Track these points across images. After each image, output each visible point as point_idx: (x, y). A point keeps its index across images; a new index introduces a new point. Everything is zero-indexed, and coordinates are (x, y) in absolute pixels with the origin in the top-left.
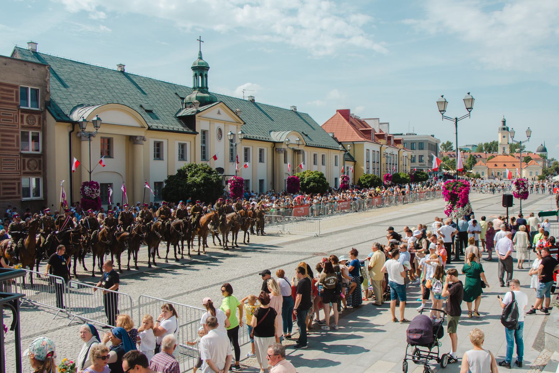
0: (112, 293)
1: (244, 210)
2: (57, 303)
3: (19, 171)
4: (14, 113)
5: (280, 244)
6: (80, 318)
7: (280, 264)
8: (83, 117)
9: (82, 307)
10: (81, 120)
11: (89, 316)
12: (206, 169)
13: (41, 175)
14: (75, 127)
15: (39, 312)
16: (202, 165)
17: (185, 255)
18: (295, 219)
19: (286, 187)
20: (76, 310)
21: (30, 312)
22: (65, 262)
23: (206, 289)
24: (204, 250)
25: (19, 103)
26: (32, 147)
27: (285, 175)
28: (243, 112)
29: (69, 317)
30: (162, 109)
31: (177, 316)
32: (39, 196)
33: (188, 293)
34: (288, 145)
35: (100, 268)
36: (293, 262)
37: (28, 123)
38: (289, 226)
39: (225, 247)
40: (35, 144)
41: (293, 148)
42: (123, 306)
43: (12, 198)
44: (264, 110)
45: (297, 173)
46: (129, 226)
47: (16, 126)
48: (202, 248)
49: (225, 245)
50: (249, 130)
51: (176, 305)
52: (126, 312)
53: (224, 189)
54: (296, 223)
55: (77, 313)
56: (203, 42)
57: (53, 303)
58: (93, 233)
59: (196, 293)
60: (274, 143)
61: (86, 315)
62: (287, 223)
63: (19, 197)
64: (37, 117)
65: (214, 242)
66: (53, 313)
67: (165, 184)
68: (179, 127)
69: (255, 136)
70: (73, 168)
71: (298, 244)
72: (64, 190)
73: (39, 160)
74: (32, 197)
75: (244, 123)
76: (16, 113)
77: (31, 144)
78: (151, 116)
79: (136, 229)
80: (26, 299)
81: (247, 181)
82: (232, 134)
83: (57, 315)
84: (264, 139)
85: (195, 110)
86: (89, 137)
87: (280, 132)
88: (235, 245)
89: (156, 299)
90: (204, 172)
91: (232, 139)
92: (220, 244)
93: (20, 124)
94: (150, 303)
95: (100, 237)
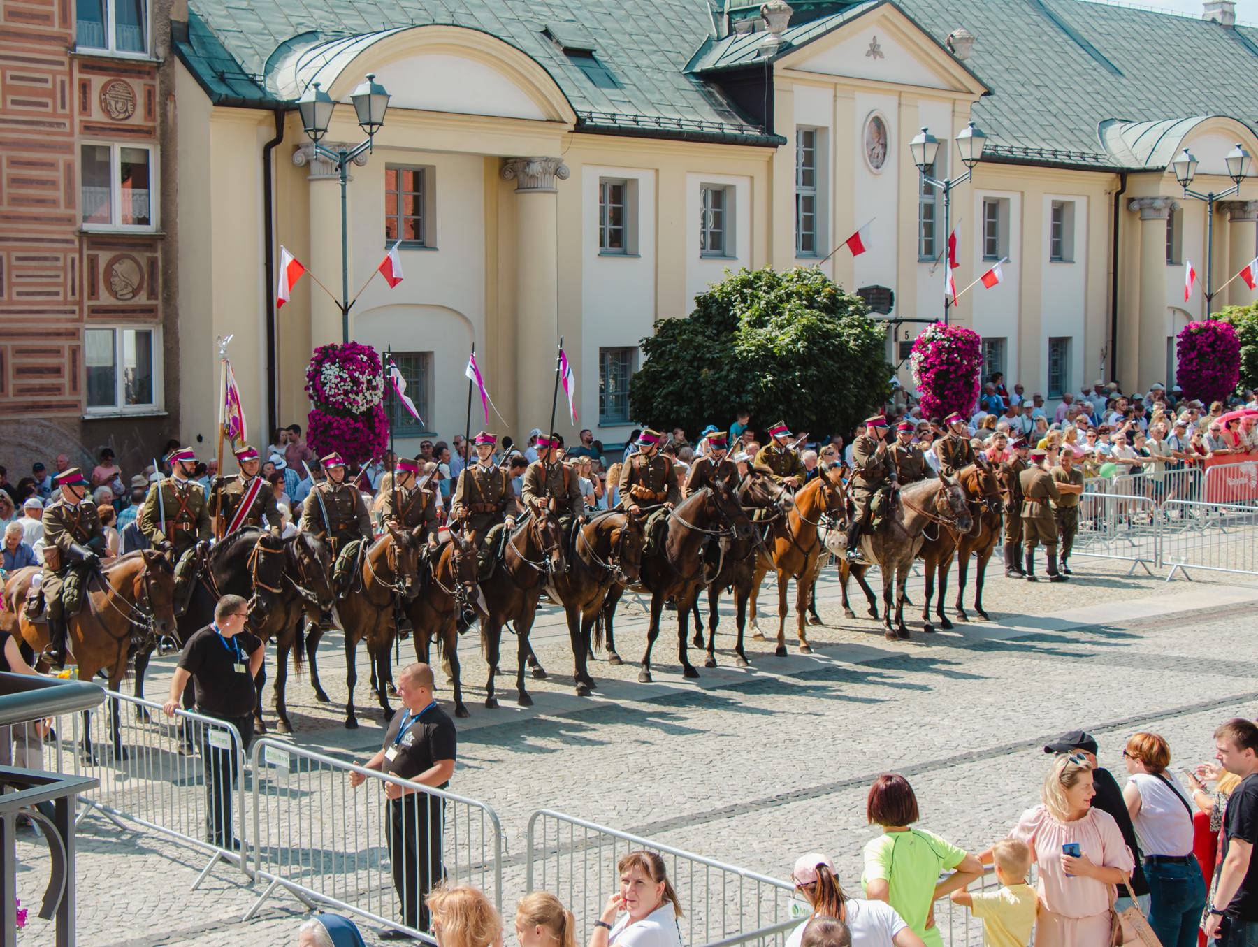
0: (422, 795)
1: (979, 465)
2: (209, 827)
3: (74, 303)
4: (54, 73)
5: (1139, 623)
6: (296, 892)
7: (1141, 710)
8: (317, 86)
9: (306, 846)
10: (309, 97)
11: (329, 883)
12: (818, 292)
13: (156, 317)
14: (286, 125)
15: (141, 858)
16: (799, 276)
17: (722, 652)
18: (1215, 515)
19: (1176, 368)
20: (281, 856)
21: (106, 856)
22: (245, 663)
23: (810, 801)
24: (802, 636)
25: (74, 32)
26: (123, 209)
27: (1168, 315)
28: (981, 39)
29: (252, 882)
30: (636, 42)
31: (677, 909)
32: (150, 401)
33: (730, 812)
34: (1185, 182)
35: (377, 693)
36: (1204, 707)
37: (107, 112)
38: (1182, 544)
39: (896, 627)
40: (133, 195)
41: (1211, 196)
42: (466, 852)
43: (48, 406)
44: (1077, 27)
45: (1228, 308)
46: (495, 528)
47: (64, 124)
48: (796, 627)
49: (892, 617)
50: (1006, 123)
51: (679, 860)
52: (476, 877)
53: (894, 379)
54: (1216, 531)
55: (285, 870)
57: (192, 827)
58: (343, 553)
59: (765, 815)
60: (1123, 174)
61: (317, 880)
62: (1174, 531)
63: (74, 406)
64: (138, 85)
65: (846, 604)
66: (194, 863)
67: (642, 358)
68: (706, 116)
69: (1035, 145)
70: (282, 290)
71: (1225, 627)
72: (230, 375)
73: (149, 258)
74: (122, 407)
75: (983, 90)
76: (61, 73)
77: (120, 197)
78: (589, 71)
79: (520, 536)
80: (93, 804)
81: (996, 344)
82: (930, 139)
83: (209, 873)
84: (1076, 160)
85: (769, 40)
86: (341, 166)
87: (1150, 124)
88: (939, 620)
89: (600, 831)
90: (807, 307)
91: (929, 161)
92: (873, 611)
93: (77, 118)
94: (574, 847)
95: (369, 568)
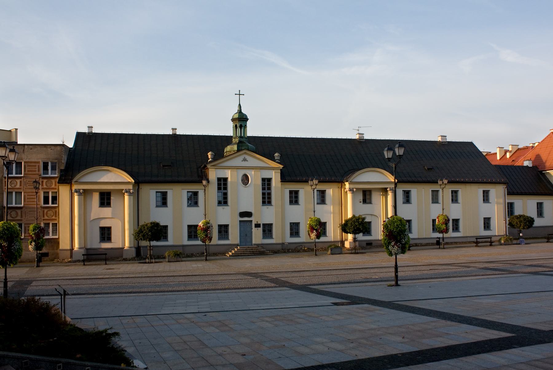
37: (47, 186)
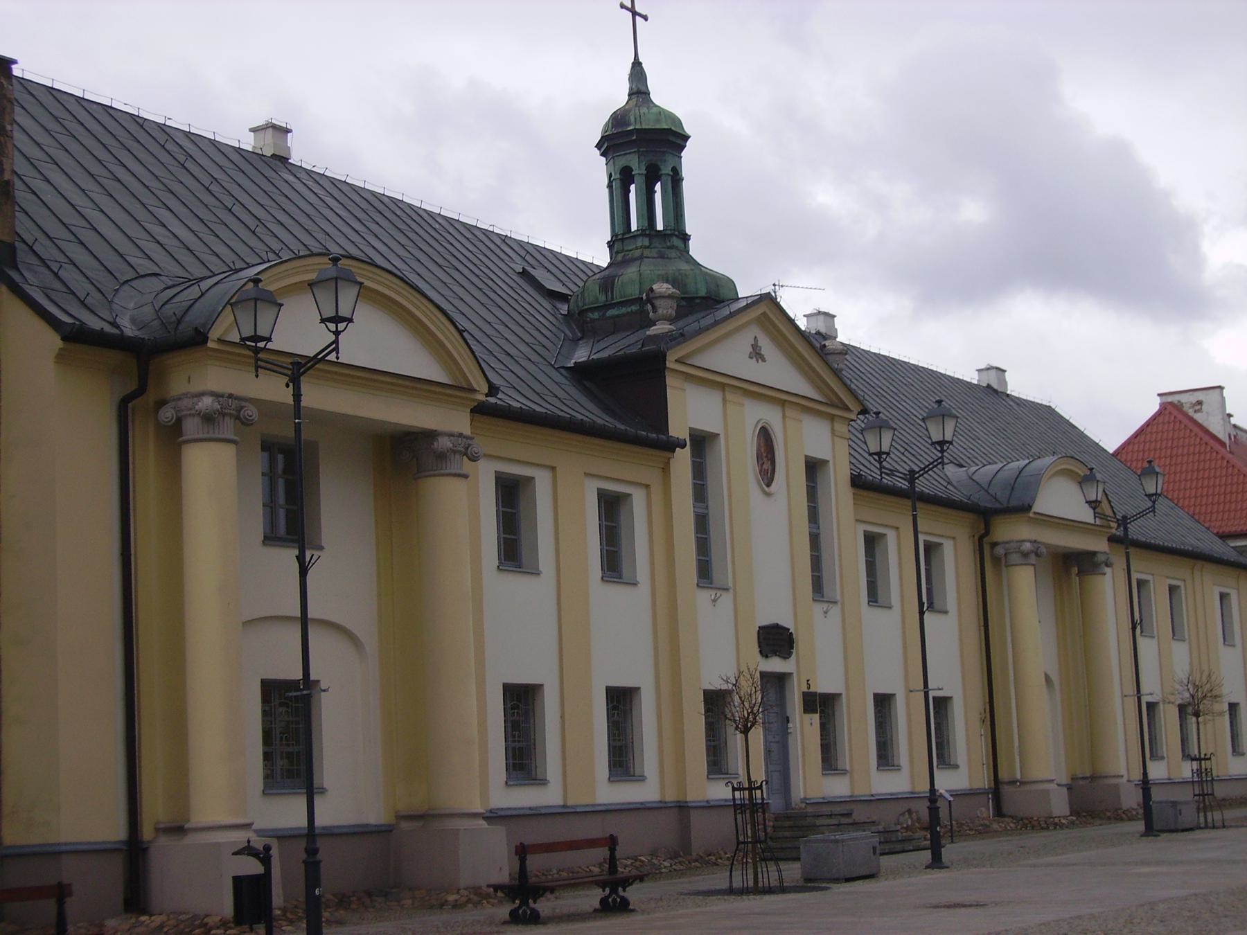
32: (765, 312)
56: (645, 18)
